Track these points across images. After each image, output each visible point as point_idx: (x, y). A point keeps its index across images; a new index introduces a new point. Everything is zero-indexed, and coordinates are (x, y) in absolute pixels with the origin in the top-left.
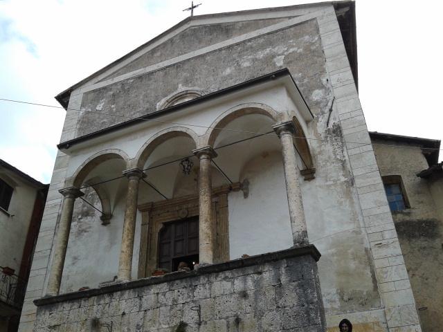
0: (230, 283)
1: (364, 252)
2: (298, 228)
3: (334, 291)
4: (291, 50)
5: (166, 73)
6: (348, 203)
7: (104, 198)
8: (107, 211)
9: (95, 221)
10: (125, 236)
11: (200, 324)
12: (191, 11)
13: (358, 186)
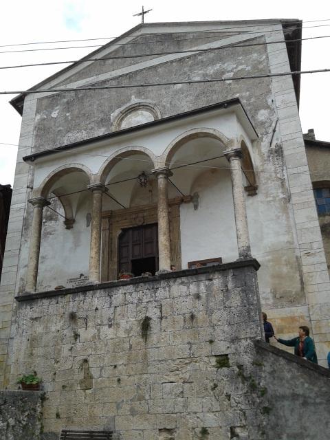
0: (186, 287)
1: (295, 259)
2: (243, 244)
3: (268, 290)
4: (240, 68)
5: (113, 62)
6: (284, 218)
7: (67, 205)
8: (69, 217)
9: (59, 224)
10: (93, 244)
11: (161, 318)
12: (141, 16)
13: (294, 203)
